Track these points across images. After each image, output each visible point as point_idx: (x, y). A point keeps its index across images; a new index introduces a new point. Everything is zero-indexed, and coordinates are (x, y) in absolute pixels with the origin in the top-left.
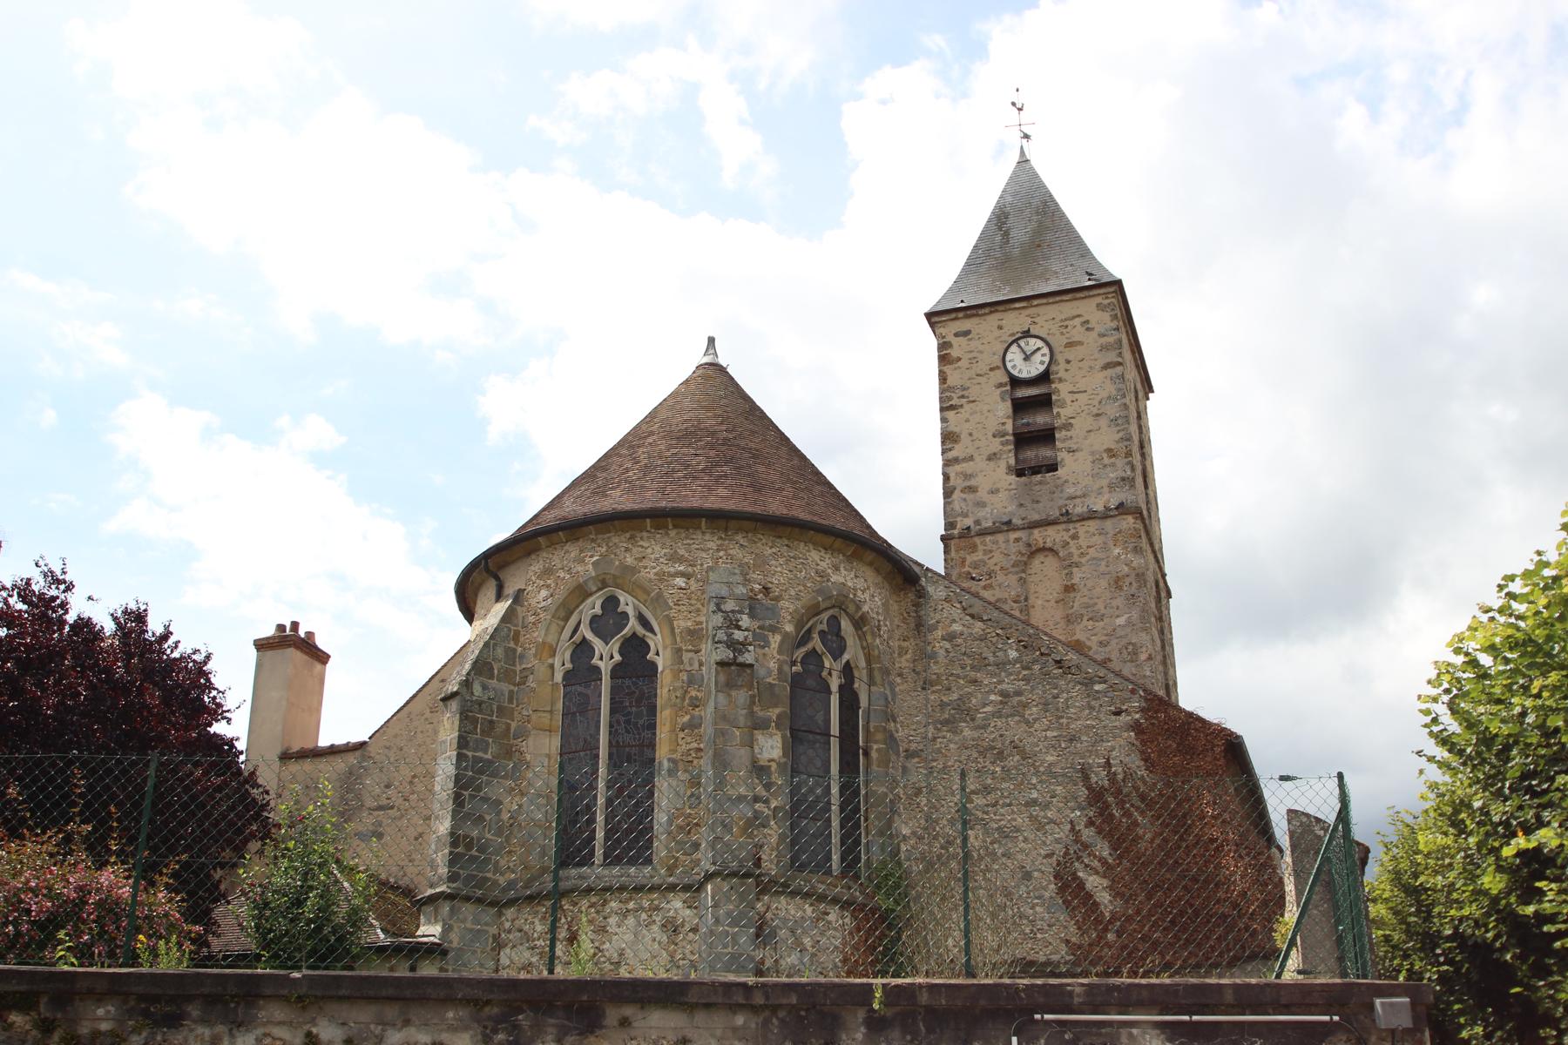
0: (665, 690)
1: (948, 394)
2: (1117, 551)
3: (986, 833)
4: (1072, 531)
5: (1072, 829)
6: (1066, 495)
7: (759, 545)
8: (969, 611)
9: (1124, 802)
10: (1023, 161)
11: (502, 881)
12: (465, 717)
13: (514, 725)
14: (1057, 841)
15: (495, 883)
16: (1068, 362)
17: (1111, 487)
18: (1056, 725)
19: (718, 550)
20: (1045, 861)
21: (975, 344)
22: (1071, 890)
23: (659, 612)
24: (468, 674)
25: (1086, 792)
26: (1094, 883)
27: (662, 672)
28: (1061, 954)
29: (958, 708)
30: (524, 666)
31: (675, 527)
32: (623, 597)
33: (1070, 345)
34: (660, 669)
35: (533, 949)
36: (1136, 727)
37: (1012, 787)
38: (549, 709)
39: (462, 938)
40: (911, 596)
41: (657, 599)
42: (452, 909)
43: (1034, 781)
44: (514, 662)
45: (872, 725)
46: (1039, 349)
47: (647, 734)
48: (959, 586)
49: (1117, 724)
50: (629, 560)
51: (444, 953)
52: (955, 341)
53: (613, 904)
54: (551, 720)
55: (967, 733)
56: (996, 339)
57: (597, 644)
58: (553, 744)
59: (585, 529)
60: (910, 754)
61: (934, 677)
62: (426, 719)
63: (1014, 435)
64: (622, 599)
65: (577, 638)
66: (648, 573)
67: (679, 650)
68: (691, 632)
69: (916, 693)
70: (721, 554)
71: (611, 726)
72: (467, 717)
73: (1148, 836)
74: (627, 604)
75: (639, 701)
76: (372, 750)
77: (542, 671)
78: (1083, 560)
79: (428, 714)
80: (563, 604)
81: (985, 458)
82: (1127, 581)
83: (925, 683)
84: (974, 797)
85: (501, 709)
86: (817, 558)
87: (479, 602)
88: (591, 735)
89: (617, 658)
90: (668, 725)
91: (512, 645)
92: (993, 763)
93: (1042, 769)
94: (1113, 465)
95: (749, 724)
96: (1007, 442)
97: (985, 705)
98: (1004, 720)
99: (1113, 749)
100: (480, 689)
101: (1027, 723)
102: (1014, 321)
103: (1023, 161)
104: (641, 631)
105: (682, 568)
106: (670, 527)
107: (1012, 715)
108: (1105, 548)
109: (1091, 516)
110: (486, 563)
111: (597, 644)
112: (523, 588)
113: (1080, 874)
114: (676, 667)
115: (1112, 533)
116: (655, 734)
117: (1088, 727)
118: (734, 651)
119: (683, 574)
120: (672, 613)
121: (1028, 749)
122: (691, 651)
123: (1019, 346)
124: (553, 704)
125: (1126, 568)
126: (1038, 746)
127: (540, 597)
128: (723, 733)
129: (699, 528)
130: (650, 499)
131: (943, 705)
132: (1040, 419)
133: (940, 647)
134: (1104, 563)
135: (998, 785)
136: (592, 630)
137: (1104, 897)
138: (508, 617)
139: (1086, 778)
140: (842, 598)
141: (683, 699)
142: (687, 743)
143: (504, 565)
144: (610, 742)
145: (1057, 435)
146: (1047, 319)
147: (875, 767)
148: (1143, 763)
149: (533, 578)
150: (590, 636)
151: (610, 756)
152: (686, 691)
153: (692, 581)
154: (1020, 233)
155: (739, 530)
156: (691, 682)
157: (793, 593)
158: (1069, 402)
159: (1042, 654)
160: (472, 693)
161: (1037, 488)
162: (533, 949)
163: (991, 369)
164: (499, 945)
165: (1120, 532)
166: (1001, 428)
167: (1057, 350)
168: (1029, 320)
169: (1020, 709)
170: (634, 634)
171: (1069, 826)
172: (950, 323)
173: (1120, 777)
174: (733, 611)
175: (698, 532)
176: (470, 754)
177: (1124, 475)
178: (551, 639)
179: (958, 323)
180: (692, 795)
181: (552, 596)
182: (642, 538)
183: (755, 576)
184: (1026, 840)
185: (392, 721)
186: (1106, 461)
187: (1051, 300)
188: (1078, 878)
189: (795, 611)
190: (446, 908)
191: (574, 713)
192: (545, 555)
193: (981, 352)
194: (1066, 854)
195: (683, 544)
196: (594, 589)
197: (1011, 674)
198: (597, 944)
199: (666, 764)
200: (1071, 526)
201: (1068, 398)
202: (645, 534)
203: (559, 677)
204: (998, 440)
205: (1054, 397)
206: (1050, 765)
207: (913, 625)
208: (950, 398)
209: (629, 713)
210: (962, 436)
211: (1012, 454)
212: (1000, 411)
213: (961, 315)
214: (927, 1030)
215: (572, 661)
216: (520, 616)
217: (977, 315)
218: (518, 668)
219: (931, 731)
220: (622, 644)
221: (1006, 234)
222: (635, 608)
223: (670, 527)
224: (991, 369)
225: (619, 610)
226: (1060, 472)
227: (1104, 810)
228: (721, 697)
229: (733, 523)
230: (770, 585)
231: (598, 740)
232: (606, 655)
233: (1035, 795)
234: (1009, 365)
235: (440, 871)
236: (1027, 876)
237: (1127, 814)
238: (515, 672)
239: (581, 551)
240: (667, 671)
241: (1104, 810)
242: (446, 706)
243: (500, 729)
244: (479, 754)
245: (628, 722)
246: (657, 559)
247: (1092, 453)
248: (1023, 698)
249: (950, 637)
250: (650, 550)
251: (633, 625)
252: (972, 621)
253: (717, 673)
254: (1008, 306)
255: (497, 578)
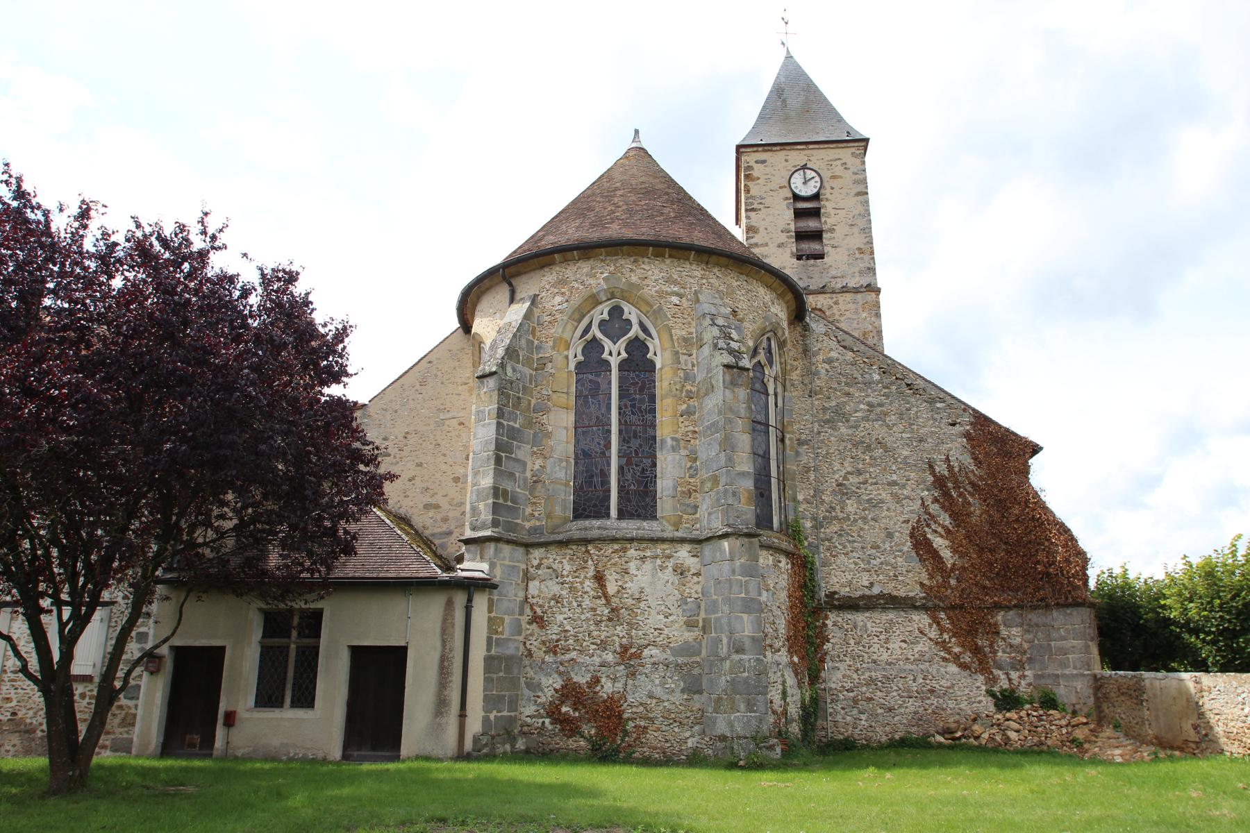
0: (665, 384)
1: (751, 200)
2: (864, 315)
3: (859, 503)
4: (835, 299)
6: (830, 276)
7: (729, 278)
10: (789, 57)
11: (527, 525)
13: (533, 402)
14: (912, 512)
15: (523, 527)
16: (832, 188)
17: (861, 273)
18: (909, 429)
20: (903, 525)
21: (768, 170)
22: (922, 546)
24: (503, 358)
25: (932, 479)
27: (661, 369)
28: (916, 592)
29: (836, 412)
30: (540, 355)
31: (670, 256)
32: (627, 308)
33: (833, 177)
34: (658, 366)
36: (967, 435)
37: (878, 471)
38: (565, 391)
39: (503, 572)
43: (894, 468)
44: (533, 351)
45: (785, 420)
46: (813, 178)
48: (835, 326)
50: (634, 279)
51: (495, 586)
53: (632, 551)
54: (568, 399)
55: (843, 430)
56: (784, 168)
57: (607, 343)
58: (569, 419)
61: (818, 388)
62: (417, 390)
63: (796, 232)
64: (626, 310)
65: (589, 336)
66: (650, 291)
67: (677, 353)
68: (685, 340)
69: (804, 399)
70: (704, 281)
71: (620, 408)
73: (978, 512)
75: (642, 390)
77: (559, 360)
78: (842, 319)
79: (418, 387)
80: (578, 309)
81: (776, 245)
82: (871, 334)
83: (811, 392)
84: (850, 477)
85: (525, 388)
86: (763, 293)
87: (479, 308)
89: (624, 355)
90: (670, 410)
91: (531, 338)
92: (863, 453)
93: (899, 460)
94: (862, 259)
95: (748, 415)
97: (856, 411)
98: (871, 423)
100: (511, 371)
101: (888, 426)
102: (797, 157)
103: (789, 57)
104: (642, 335)
105: (676, 289)
106: (667, 256)
108: (856, 312)
109: (845, 290)
111: (607, 343)
113: (929, 536)
114: (675, 366)
115: (861, 303)
117: (932, 432)
118: (734, 357)
119: (677, 294)
120: (670, 323)
124: (569, 387)
125: (870, 327)
126: (896, 443)
128: (730, 421)
130: (644, 231)
131: (825, 409)
133: (822, 368)
134: (856, 322)
135: (867, 469)
137: (946, 554)
138: (528, 316)
139: (931, 467)
142: (685, 427)
143: (518, 274)
146: (818, 158)
147: (788, 451)
148: (972, 461)
150: (599, 335)
151: (620, 432)
152: (683, 386)
153: (684, 300)
154: (795, 102)
155: (717, 264)
156: (686, 378)
157: (751, 317)
159: (897, 379)
160: (506, 374)
161: (811, 269)
163: (780, 188)
164: (527, 577)
165: (866, 303)
166: (787, 227)
167: (825, 180)
168: (806, 158)
169: (882, 416)
170: (637, 338)
171: (920, 502)
172: (753, 154)
173: (956, 469)
174: (724, 326)
175: (687, 262)
176: (505, 423)
177: (869, 266)
178: (567, 335)
181: (567, 301)
182: (643, 263)
183: (727, 301)
184: (888, 509)
185: (387, 390)
186: (857, 255)
187: (822, 146)
189: (754, 331)
191: (586, 397)
192: (558, 269)
193: (774, 176)
194: (919, 521)
195: (676, 271)
196: (604, 299)
197: (875, 391)
199: (669, 442)
200: (834, 295)
201: (833, 212)
202: (646, 260)
203: (572, 366)
204: (785, 234)
205: (822, 211)
206: (906, 457)
208: (752, 204)
209: (634, 399)
210: (760, 229)
211: (794, 245)
212: (786, 215)
213: (760, 149)
214: (1054, 709)
217: (771, 151)
220: (628, 345)
221: (784, 101)
222: (638, 317)
223: (667, 256)
224: (780, 188)
226: (826, 259)
227: (946, 494)
229: (714, 259)
230: (737, 309)
231: (609, 419)
232: (614, 352)
233: (895, 477)
234: (793, 186)
235: (483, 517)
236: (890, 535)
239: (592, 268)
241: (946, 494)
243: (524, 404)
245: (633, 406)
246: (656, 280)
247: (848, 250)
248: (884, 409)
249: (829, 361)
250: (650, 273)
251: (635, 330)
252: (844, 351)
253: (724, 373)
254: (792, 147)
255: (510, 284)
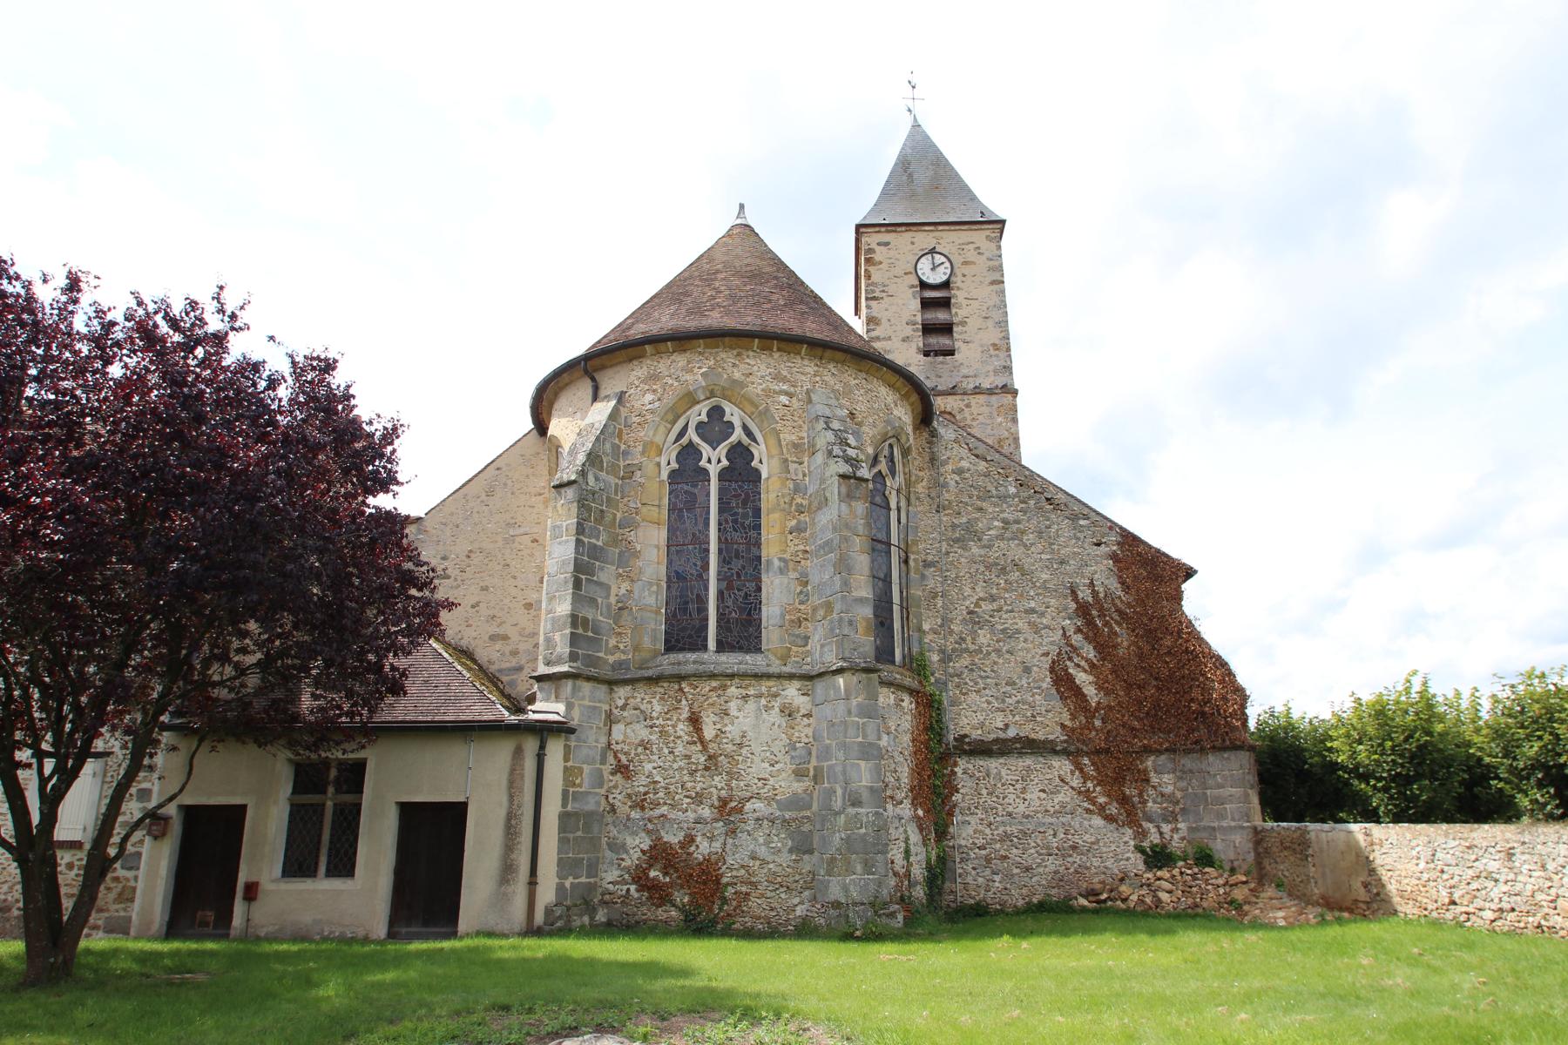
2: (999, 419)
3: (993, 633)
4: (966, 401)
5: (1064, 634)
6: (962, 374)
7: (846, 375)
8: (975, 452)
9: (1105, 616)
10: (916, 126)
11: (611, 659)
12: (582, 503)
13: (619, 515)
14: (1052, 643)
15: (606, 661)
16: (964, 276)
19: (815, 375)
21: (892, 253)
22: (1063, 682)
23: (765, 424)
24: (584, 465)
26: (1082, 678)
28: (1057, 735)
29: (967, 530)
30: (627, 462)
31: (779, 350)
32: (728, 408)
33: (965, 263)
35: (651, 727)
38: (657, 503)
39: (582, 714)
40: (926, 435)
41: (765, 414)
42: (574, 688)
45: (910, 538)
47: (753, 534)
48: (966, 431)
49: (1098, 552)
50: (737, 375)
51: (572, 731)
52: (878, 249)
55: (975, 550)
57: (706, 449)
58: (660, 535)
59: (695, 342)
60: (927, 564)
61: (947, 502)
62: (482, 501)
64: (727, 410)
65: (684, 441)
66: (755, 389)
70: (818, 379)
72: (583, 505)
73: (1125, 644)
74: (733, 414)
75: (745, 503)
76: (428, 524)
77: (650, 468)
78: (974, 423)
79: (483, 497)
80: (672, 409)
82: (1007, 442)
83: (938, 507)
86: (885, 393)
88: (700, 532)
89: (725, 462)
91: (617, 441)
93: (1038, 584)
94: (997, 356)
95: (866, 533)
96: (917, 330)
97: (989, 529)
99: (1096, 572)
101: (1025, 546)
102: (925, 240)
103: (916, 126)
105: (785, 387)
107: (1012, 539)
108: (991, 417)
109: (978, 391)
110: (586, 364)
111: (706, 449)
112: (625, 390)
113: (1071, 671)
115: (996, 406)
116: (760, 534)
117: (1074, 553)
118: (851, 465)
119: (787, 393)
121: (1026, 567)
122: (796, 462)
123: (933, 258)
124: (660, 499)
127: (645, 400)
128: (846, 539)
129: (799, 353)
131: (954, 526)
132: (941, 316)
133: (952, 479)
134: (990, 427)
136: (699, 435)
137: (1090, 691)
138: (613, 416)
139: (1074, 593)
140: (899, 430)
141: (791, 505)
142: (795, 545)
144: (719, 538)
145: (955, 329)
146: (949, 241)
148: (1119, 585)
149: (636, 382)
150: (696, 439)
151: (720, 551)
152: (793, 498)
153: (794, 400)
156: (797, 489)
158: (964, 306)
161: (940, 366)
162: (651, 727)
163: (906, 274)
164: (610, 720)
166: (913, 318)
167: (956, 266)
169: (1019, 534)
170: (739, 442)
171: (1061, 632)
173: (1102, 595)
174: (839, 430)
175: (798, 357)
176: (586, 540)
178: (659, 439)
179: (880, 235)
180: (801, 592)
181: (659, 400)
182: (748, 356)
184: (1026, 641)
186: (992, 352)
188: (1070, 674)
190: (568, 685)
191: (681, 510)
192: (648, 362)
196: (702, 397)
198: (718, 726)
199: (776, 563)
200: (965, 397)
201: (965, 302)
202: (751, 353)
203: (665, 475)
204: (911, 327)
205: (953, 301)
207: (927, 459)
208: (873, 291)
209: (736, 514)
211: (921, 339)
213: (883, 229)
215: (678, 460)
216: (623, 415)
217: (895, 231)
218: (622, 464)
219: (944, 546)
221: (910, 176)
224: (906, 274)
225: (725, 419)
227: (1090, 623)
228: (844, 506)
229: (828, 353)
230: (854, 412)
231: (708, 536)
232: (714, 459)
233: (1033, 604)
234: (920, 273)
235: (558, 649)
237: (1106, 624)
238: (619, 467)
239: (689, 362)
240: (774, 479)
241: (1090, 623)
242: (560, 494)
243: (608, 517)
244: (593, 541)
245: (735, 521)
246: (762, 377)
247: (982, 346)
249: (960, 472)
250: (756, 368)
251: (738, 434)
252: (977, 460)
253: (840, 484)
255: (593, 379)
